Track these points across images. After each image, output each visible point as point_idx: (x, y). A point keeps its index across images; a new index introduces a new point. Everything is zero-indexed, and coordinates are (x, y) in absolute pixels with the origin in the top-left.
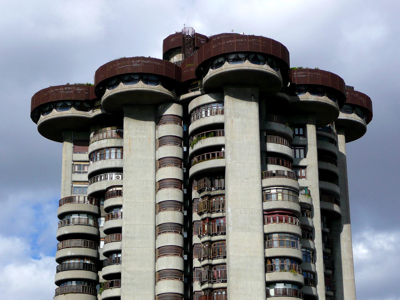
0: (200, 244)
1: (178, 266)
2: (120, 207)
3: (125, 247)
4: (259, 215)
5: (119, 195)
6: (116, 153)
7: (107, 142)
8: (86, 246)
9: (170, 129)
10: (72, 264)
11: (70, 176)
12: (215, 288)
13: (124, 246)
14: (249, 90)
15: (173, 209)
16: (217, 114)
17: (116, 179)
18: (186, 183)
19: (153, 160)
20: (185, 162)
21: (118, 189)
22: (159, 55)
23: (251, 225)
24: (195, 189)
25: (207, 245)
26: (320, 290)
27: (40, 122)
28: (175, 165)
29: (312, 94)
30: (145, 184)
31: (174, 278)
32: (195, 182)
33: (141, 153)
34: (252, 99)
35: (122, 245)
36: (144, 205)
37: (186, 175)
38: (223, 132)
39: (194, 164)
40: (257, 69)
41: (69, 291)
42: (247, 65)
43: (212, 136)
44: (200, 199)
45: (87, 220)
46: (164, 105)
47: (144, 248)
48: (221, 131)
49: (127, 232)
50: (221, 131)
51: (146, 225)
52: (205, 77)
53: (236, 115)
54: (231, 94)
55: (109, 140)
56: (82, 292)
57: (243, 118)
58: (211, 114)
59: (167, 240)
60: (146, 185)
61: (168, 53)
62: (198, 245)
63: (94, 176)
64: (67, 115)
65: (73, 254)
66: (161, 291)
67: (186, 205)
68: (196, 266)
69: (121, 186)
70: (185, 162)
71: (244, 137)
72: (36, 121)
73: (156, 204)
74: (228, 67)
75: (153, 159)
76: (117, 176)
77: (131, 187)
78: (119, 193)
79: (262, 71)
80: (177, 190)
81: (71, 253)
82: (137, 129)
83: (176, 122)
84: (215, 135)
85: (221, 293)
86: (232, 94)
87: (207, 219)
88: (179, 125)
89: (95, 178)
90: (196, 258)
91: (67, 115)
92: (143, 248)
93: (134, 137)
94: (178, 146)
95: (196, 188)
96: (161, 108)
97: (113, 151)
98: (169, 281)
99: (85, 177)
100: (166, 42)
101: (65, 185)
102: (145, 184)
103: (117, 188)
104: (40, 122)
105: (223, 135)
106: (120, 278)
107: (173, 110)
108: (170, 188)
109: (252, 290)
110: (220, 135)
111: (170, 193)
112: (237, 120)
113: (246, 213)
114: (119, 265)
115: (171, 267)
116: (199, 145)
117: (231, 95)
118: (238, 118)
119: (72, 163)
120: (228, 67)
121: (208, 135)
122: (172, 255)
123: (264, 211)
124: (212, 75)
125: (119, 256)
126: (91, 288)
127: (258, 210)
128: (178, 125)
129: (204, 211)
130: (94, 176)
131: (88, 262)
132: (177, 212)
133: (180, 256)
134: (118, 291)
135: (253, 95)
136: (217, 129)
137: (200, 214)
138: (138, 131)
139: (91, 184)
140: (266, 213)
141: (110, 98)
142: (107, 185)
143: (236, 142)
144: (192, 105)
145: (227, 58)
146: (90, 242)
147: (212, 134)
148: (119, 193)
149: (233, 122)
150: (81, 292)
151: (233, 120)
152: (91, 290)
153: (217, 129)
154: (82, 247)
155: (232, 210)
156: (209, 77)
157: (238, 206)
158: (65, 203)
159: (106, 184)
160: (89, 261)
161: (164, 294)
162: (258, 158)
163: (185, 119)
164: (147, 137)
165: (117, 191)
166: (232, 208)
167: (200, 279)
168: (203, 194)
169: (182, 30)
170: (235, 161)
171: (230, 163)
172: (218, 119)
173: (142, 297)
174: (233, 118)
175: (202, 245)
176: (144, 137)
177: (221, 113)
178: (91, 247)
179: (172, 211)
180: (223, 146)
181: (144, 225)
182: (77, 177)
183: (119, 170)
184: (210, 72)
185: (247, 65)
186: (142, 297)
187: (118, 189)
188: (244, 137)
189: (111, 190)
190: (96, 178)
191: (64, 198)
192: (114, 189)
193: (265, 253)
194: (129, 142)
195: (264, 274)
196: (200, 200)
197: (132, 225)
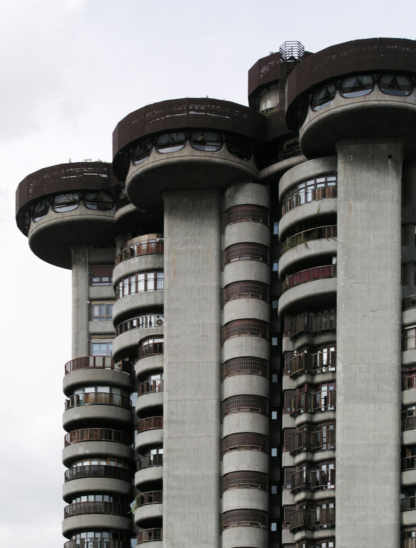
0: (294, 428)
1: (258, 466)
2: (159, 371)
3: (168, 438)
4: (393, 374)
5: (158, 351)
6: (146, 281)
7: (140, 262)
8: (108, 438)
9: (240, 232)
10: (104, 468)
11: (85, 326)
12: (317, 499)
13: (165, 437)
14: (383, 147)
15: (249, 372)
16: (324, 196)
17: (156, 325)
18: (267, 328)
19: (214, 288)
20: (267, 290)
21: (157, 341)
22: (243, 100)
23: (378, 391)
24: (287, 335)
25: (305, 429)
26: (117, 547)
27: (31, 233)
28: (252, 295)
29: (312, 127)
30: (201, 330)
31: (249, 486)
32: (287, 321)
33: (191, 278)
34: (388, 164)
35: (162, 434)
36: (199, 366)
37: (273, 311)
38: (335, 229)
39: (287, 289)
40: (394, 104)
41: (83, 511)
42: (376, 98)
43: (314, 239)
44: (295, 352)
45: (110, 396)
46: (234, 187)
47: (200, 439)
48: (332, 228)
49: (172, 413)
50: (332, 228)
51: (191, 400)
52: (302, 127)
53: (357, 197)
54: (348, 156)
55: (143, 258)
56: (105, 511)
57: (370, 201)
58: (314, 198)
59: (239, 423)
60: (203, 332)
61: (255, 95)
62: (291, 430)
63: (123, 322)
64: (71, 217)
65: (87, 452)
66: (228, 507)
67: (269, 366)
68: (286, 465)
69: (161, 336)
70: (267, 290)
71: (372, 236)
72: (25, 232)
73: (221, 364)
74: (340, 103)
75: (215, 286)
76: (159, 321)
77: (177, 336)
78: (158, 349)
79: (405, 107)
80: (256, 338)
81: (85, 450)
82: (186, 234)
83: (255, 219)
84: (320, 236)
85: (328, 506)
86: (351, 156)
87: (306, 385)
88: (262, 223)
89: (121, 325)
90: (286, 451)
91: (71, 217)
92: (199, 437)
93: (182, 248)
94: (260, 261)
95: (289, 333)
96: (229, 194)
97: (141, 277)
98: (241, 490)
99: (110, 327)
100: (254, 73)
101: (77, 341)
102: (201, 330)
103: (155, 340)
104: (31, 233)
105: (335, 235)
106: (161, 488)
107: (247, 196)
108: (243, 335)
109: (375, 500)
110: (329, 236)
111: (244, 344)
112: (360, 206)
113: (369, 372)
114: (159, 468)
115: (244, 468)
116: (288, 258)
117: (350, 158)
118: (361, 201)
119: (88, 302)
120: (340, 103)
121: (309, 237)
122: (246, 448)
123: (403, 366)
124: (312, 122)
125: (161, 451)
126: (119, 505)
127: (392, 366)
128: (260, 222)
129: (300, 371)
130: (123, 322)
131: (113, 464)
132: (255, 376)
133: (260, 449)
134: (159, 509)
135: (390, 157)
136: (323, 224)
137: (294, 377)
138: (189, 238)
139: (117, 336)
140: (407, 370)
141: (138, 179)
142: (140, 336)
143: (357, 245)
144: (285, 183)
145: (338, 86)
146: (115, 432)
147: (316, 234)
148: (158, 349)
149: (352, 208)
150: (103, 511)
151: (352, 205)
152: (119, 509)
153: (323, 224)
154: (103, 441)
155: (344, 367)
156: (308, 126)
157: (356, 360)
158: (75, 368)
159: (139, 335)
160: (116, 462)
161: (234, 512)
162: (395, 273)
163: (270, 212)
164: (204, 248)
165: (155, 345)
166: (345, 364)
167: (293, 486)
168: (299, 343)
169: (281, 49)
170: (352, 281)
171: (343, 284)
172: (326, 206)
173: (198, 517)
174: (351, 202)
175: (298, 429)
176: (200, 247)
177: (331, 194)
178: (117, 440)
179: (246, 376)
180: (334, 254)
181: (199, 400)
182: (97, 326)
183: (158, 309)
184: (310, 117)
185: (376, 98)
186: (198, 517)
187: (157, 341)
188: (372, 236)
189: (146, 343)
190: (123, 326)
191: (70, 362)
192: (151, 341)
193: (402, 439)
194: (173, 258)
195: (398, 474)
196: (295, 355)
197: (180, 400)
